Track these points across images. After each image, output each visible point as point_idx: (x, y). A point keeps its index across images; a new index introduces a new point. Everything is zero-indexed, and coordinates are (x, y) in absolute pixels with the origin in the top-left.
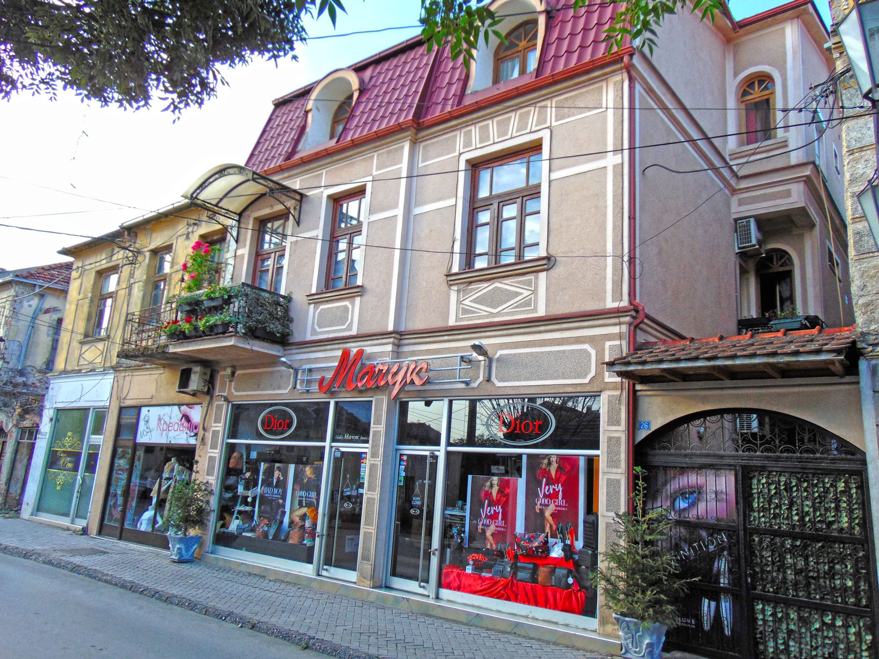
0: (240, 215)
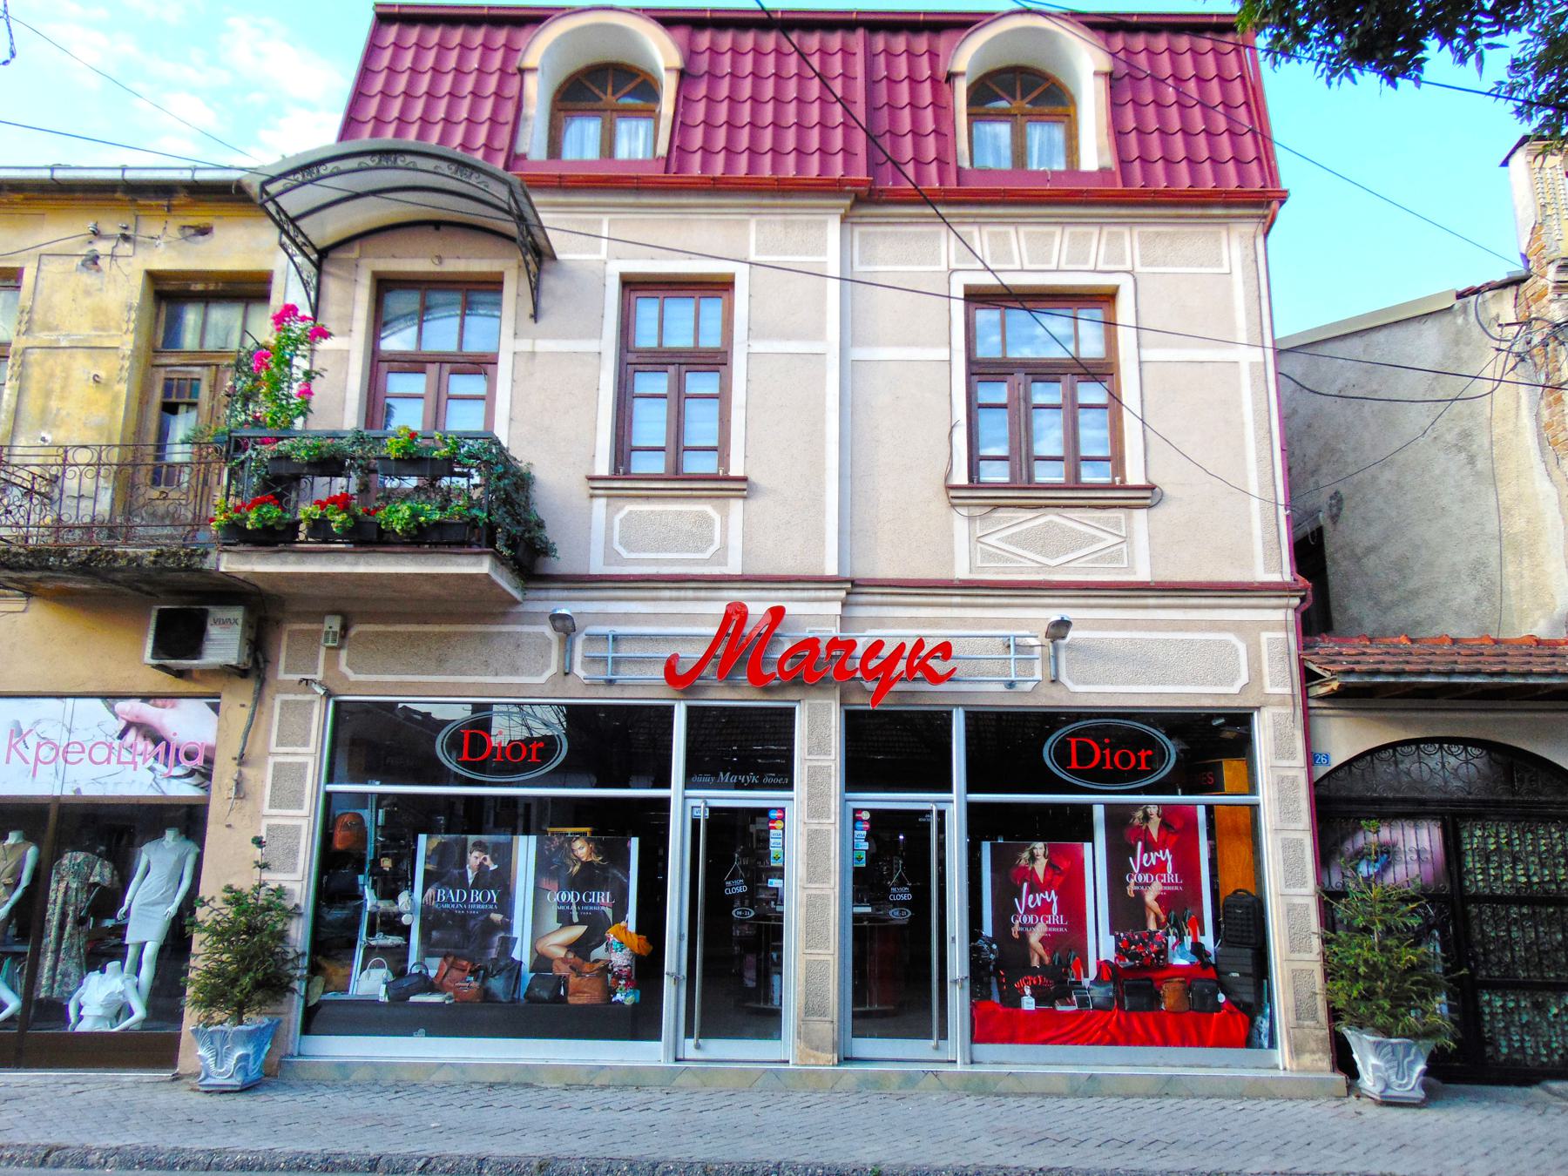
0: (324, 253)
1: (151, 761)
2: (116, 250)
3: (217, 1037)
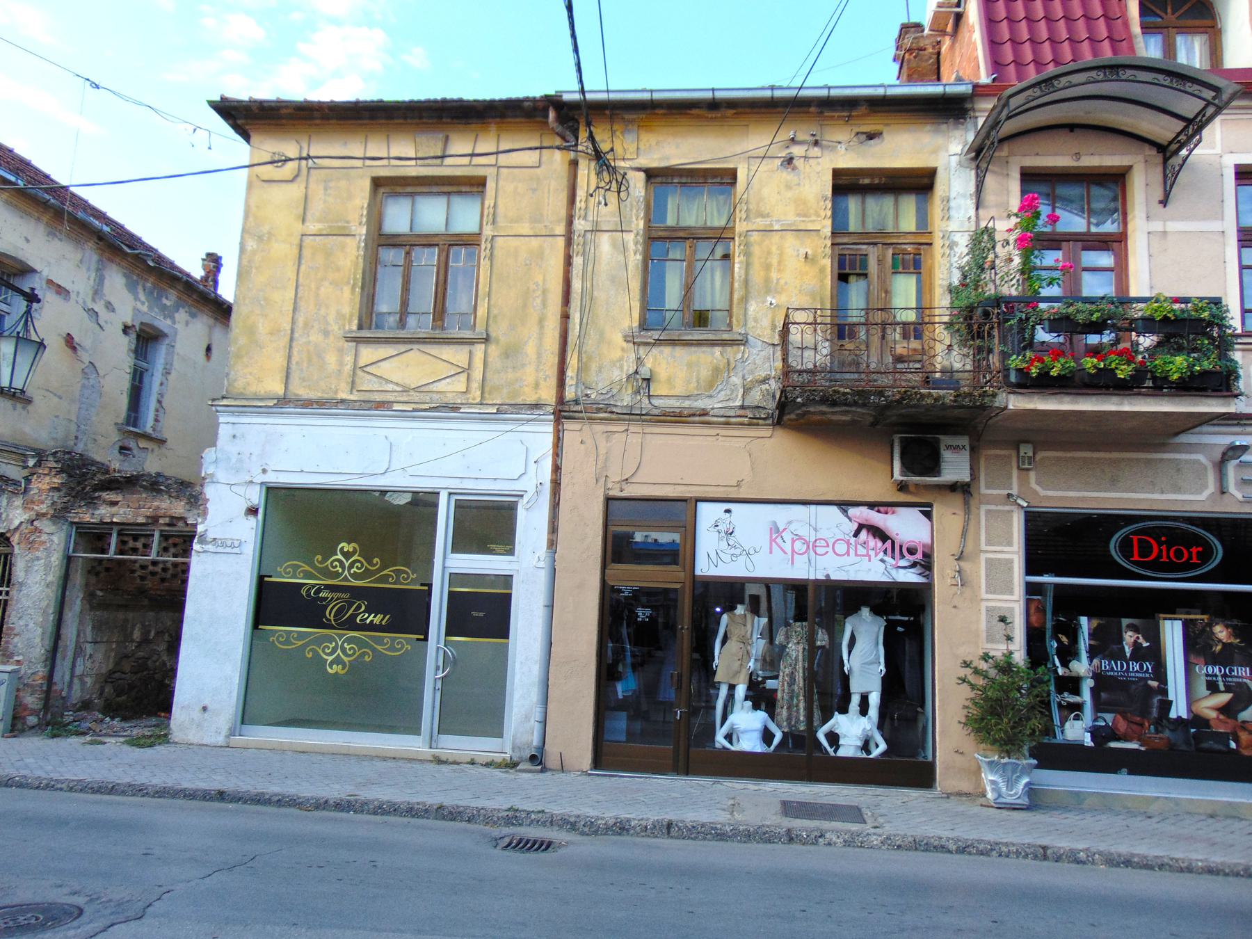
1: (881, 555)
2: (808, 152)
3: (1010, 768)
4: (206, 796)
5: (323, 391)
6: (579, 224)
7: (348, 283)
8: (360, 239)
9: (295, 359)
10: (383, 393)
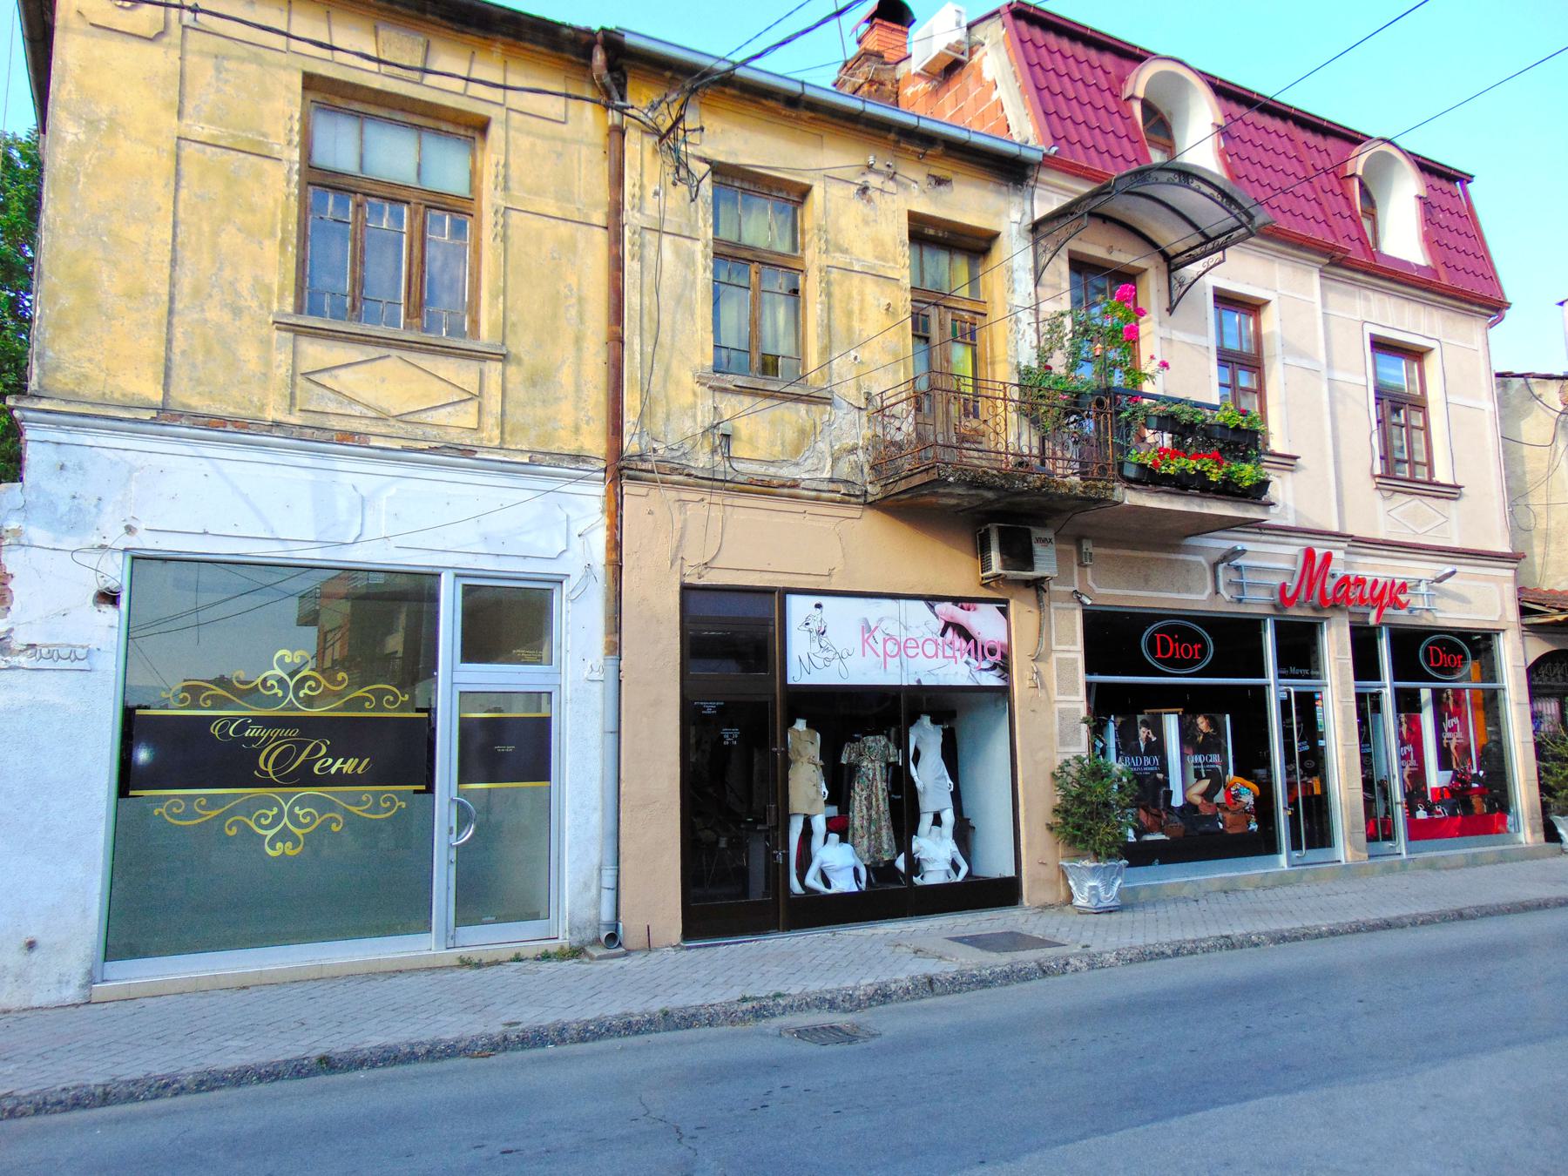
4: (298, 1070)
5: (237, 405)
6: (633, 217)
7: (273, 234)
8: (291, 169)
9: (179, 344)
10: (346, 419)
